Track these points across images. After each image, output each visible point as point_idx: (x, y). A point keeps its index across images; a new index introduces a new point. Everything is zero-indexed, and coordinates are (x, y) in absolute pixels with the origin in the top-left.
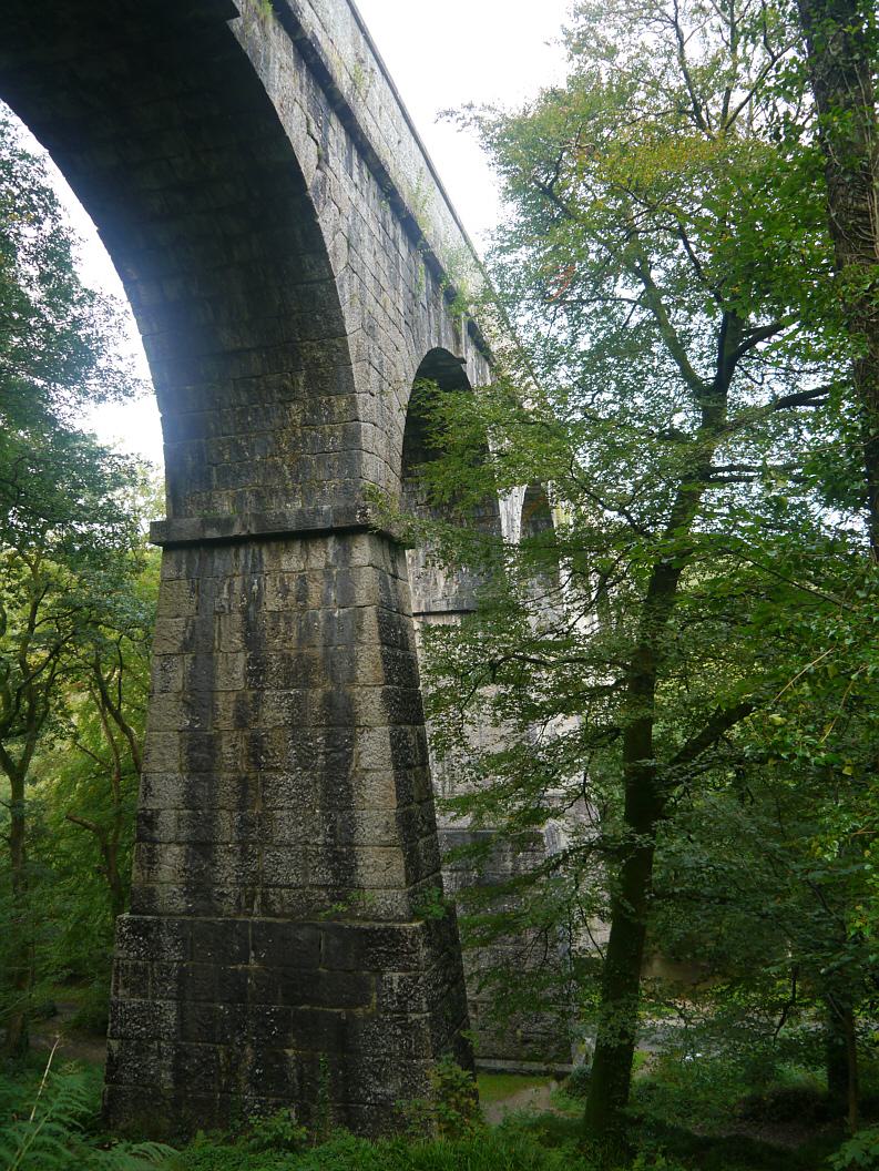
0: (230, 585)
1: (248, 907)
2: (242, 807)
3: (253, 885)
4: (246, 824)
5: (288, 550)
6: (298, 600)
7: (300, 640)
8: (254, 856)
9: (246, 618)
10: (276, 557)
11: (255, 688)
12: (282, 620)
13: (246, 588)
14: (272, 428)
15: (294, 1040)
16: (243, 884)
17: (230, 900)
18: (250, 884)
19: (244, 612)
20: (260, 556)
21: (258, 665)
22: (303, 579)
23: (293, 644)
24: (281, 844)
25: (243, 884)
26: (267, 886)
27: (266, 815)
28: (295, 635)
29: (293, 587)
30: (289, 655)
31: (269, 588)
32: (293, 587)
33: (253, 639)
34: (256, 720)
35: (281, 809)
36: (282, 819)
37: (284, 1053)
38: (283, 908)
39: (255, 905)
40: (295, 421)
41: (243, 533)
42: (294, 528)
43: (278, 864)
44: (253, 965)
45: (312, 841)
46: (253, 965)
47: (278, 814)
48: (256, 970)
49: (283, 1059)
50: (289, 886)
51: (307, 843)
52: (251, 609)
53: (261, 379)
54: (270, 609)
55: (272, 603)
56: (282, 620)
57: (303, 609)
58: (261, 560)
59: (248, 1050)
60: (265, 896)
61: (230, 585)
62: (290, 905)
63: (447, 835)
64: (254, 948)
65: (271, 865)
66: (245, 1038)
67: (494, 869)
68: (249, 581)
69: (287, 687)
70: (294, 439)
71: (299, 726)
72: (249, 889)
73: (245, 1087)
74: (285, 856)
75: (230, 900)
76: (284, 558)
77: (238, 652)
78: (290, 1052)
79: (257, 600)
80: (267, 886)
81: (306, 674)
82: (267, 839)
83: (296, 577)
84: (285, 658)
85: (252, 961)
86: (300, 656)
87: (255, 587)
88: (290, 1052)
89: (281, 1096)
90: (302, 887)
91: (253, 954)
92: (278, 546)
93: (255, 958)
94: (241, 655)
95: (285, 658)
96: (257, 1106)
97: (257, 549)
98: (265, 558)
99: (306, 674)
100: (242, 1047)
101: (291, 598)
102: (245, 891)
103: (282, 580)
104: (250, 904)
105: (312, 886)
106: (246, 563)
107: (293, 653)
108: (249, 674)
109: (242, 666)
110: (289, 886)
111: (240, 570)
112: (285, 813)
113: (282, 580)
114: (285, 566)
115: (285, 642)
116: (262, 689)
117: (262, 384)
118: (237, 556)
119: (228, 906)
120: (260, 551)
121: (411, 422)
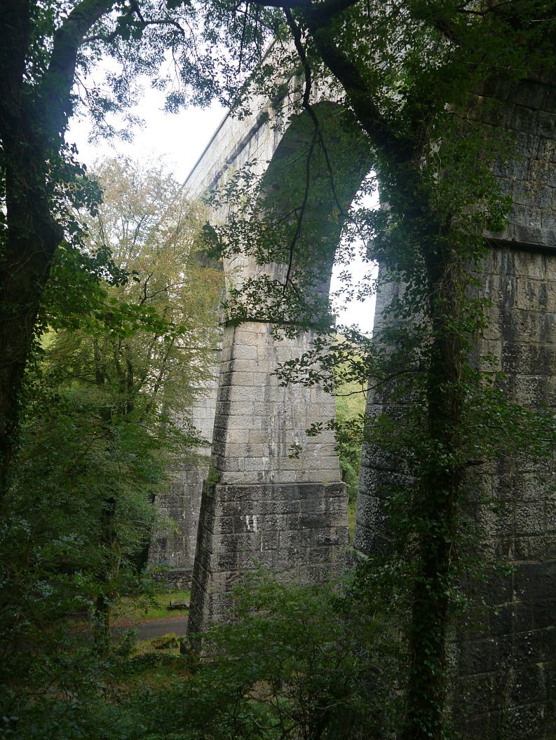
0: (491, 282)
1: (504, 554)
2: (500, 471)
3: (508, 535)
4: (504, 485)
5: (533, 260)
6: (541, 303)
7: (542, 337)
8: (510, 512)
9: (503, 312)
10: (525, 264)
11: (510, 372)
12: (529, 317)
13: (503, 286)
14: (529, 156)
15: (544, 655)
16: (501, 536)
17: (491, 550)
18: (507, 535)
19: (501, 306)
20: (513, 262)
21: (512, 353)
22: (544, 288)
23: (537, 338)
24: (529, 501)
25: (501, 536)
26: (519, 535)
27: (519, 478)
28: (538, 330)
29: (537, 291)
30: (535, 347)
31: (519, 290)
32: (537, 291)
33: (508, 331)
34: (511, 399)
35: (529, 472)
36: (529, 480)
37: (537, 667)
38: (529, 551)
39: (510, 552)
40: (546, 156)
41: (510, 239)
42: (547, 245)
43: (527, 516)
44: (516, 601)
45: (550, 497)
46: (516, 601)
47: (527, 476)
48: (518, 605)
49: (534, 671)
50: (534, 534)
51: (547, 498)
52: (507, 305)
53: (536, 112)
54: (520, 307)
55: (522, 302)
56: (529, 317)
57: (543, 312)
58: (514, 266)
59: (511, 671)
60: (517, 543)
61: (491, 282)
62: (534, 549)
63: (282, 488)
64: (516, 589)
65: (522, 518)
66: (509, 662)
67: (313, 511)
68: (505, 281)
69: (532, 373)
70: (542, 170)
71: (541, 405)
72: (506, 539)
73: (509, 701)
74: (532, 510)
75: (491, 550)
76: (531, 267)
77: (496, 340)
78: (540, 665)
79: (509, 298)
80: (519, 535)
81: (546, 364)
82: (519, 496)
83: (539, 284)
84: (533, 349)
85: (514, 598)
86: (542, 349)
87: (510, 287)
88: (540, 665)
89: (535, 701)
90: (543, 534)
91: (515, 593)
92: (525, 256)
93: (516, 595)
94: (499, 343)
95: (533, 349)
96: (517, 714)
97: (510, 255)
98: (517, 263)
99: (546, 364)
100: (507, 670)
101: (535, 301)
102: (502, 541)
103: (529, 284)
104: (506, 552)
105: (549, 532)
106: (503, 265)
107: (537, 346)
108: (505, 359)
109: (500, 352)
110: (534, 534)
111: (498, 270)
112: (532, 475)
113: (529, 284)
114: (531, 274)
115: (531, 336)
116: (515, 374)
117: (535, 117)
118: (495, 257)
119: (489, 554)
120: (513, 257)
121: (240, 152)
